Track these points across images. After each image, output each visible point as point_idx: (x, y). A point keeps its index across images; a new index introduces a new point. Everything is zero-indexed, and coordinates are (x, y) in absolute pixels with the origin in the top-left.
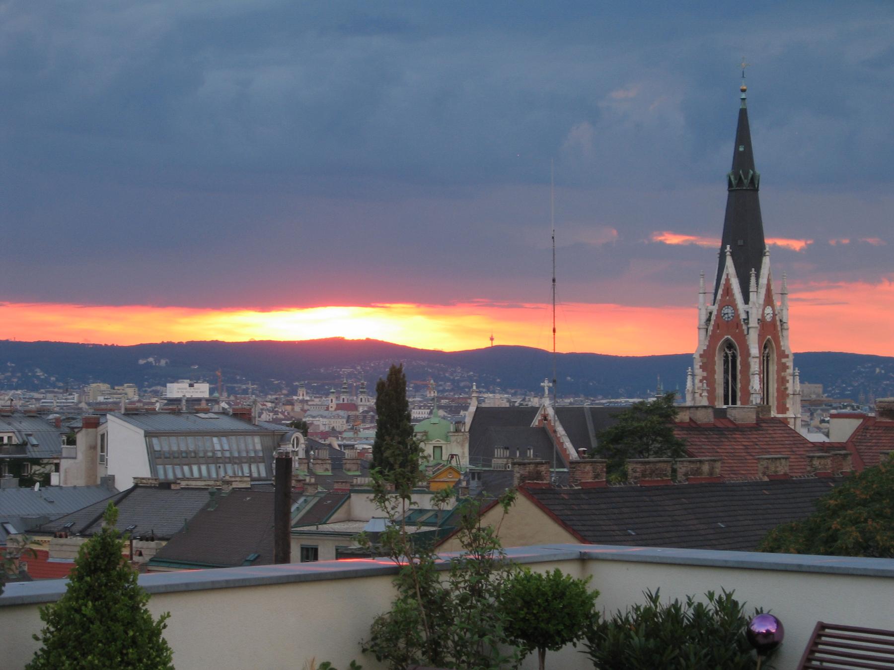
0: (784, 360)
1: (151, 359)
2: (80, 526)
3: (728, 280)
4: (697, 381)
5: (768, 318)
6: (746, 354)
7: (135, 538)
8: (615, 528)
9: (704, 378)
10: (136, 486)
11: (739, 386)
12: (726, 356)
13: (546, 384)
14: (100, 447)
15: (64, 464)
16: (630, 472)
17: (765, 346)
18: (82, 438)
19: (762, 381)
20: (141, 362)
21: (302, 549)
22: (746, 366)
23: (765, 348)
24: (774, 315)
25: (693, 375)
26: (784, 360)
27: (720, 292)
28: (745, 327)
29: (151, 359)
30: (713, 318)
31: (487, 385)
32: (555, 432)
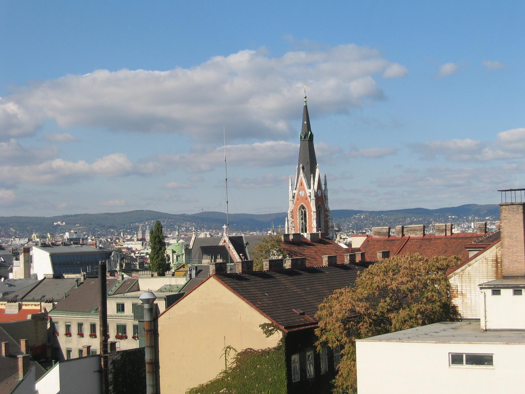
0: (326, 213)
1: (59, 223)
2: (19, 297)
3: (301, 179)
4: (289, 223)
5: (320, 195)
6: (310, 211)
7: (43, 301)
8: (258, 292)
9: (293, 222)
10: (45, 278)
11: (308, 224)
12: (302, 212)
13: (225, 227)
14: (28, 261)
15: (14, 269)
16: (264, 265)
17: (318, 207)
18: (22, 257)
19: (317, 222)
20: (55, 224)
21: (117, 304)
22: (310, 216)
23: (318, 208)
24: (322, 194)
25: (288, 221)
26: (326, 213)
27: (298, 184)
28: (309, 199)
29: (59, 223)
30: (296, 196)
31: (200, 228)
32: (229, 247)
